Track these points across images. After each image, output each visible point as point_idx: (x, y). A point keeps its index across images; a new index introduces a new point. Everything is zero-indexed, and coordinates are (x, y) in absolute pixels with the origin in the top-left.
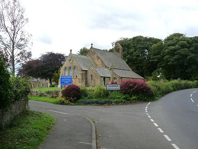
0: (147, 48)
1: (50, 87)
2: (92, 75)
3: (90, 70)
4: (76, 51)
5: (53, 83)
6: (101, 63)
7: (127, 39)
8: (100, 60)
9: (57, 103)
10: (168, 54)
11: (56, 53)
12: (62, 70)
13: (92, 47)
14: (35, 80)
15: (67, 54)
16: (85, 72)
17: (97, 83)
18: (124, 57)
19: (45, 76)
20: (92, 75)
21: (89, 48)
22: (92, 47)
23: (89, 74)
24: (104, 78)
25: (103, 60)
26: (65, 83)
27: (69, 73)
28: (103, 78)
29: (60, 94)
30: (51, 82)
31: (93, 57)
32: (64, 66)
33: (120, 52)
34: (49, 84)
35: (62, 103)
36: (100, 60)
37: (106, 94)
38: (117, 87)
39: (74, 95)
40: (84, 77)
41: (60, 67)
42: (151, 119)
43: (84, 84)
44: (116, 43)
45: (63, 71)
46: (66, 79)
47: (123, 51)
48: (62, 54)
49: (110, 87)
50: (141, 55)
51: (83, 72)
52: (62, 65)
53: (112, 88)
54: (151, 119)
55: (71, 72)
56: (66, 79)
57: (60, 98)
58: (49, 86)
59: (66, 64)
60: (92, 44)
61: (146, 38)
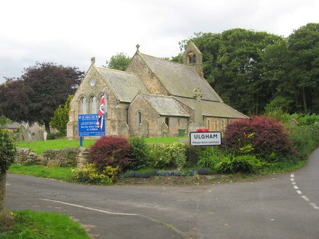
0: (252, 55)
1: (48, 139)
2: (140, 113)
3: (136, 101)
4: (102, 62)
5: (55, 131)
6: (157, 86)
7: (210, 35)
8: (155, 81)
9: (72, 180)
10: (298, 65)
11: (58, 65)
12: (74, 101)
13: (138, 51)
14: (16, 125)
15: (82, 65)
16: (125, 106)
17: (153, 129)
18: (206, 74)
19: (31, 116)
20: (140, 113)
21: (130, 54)
22: (138, 51)
23: (134, 110)
24: (167, 118)
25: (161, 78)
26: (89, 131)
27: (89, 110)
28: (164, 118)
29: (81, 159)
30: (48, 129)
31: (140, 74)
32: (77, 94)
33: (197, 62)
34: (45, 134)
35: (83, 179)
36: (155, 81)
37: (193, 154)
38: (215, 139)
39: (123, 160)
40: (123, 118)
41: (67, 96)
42: (311, 204)
43: (127, 131)
44: (189, 42)
45: (77, 103)
46: (92, 121)
47: (204, 60)
48: (73, 67)
49: (198, 140)
50: (234, 65)
51: (119, 106)
52: (73, 92)
53: (202, 140)
54: (311, 204)
55: (94, 104)
56: (92, 121)
57: (83, 167)
58: (45, 138)
59: (82, 89)
60: (138, 46)
61: (250, 33)
